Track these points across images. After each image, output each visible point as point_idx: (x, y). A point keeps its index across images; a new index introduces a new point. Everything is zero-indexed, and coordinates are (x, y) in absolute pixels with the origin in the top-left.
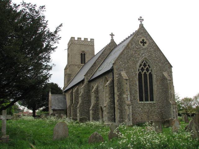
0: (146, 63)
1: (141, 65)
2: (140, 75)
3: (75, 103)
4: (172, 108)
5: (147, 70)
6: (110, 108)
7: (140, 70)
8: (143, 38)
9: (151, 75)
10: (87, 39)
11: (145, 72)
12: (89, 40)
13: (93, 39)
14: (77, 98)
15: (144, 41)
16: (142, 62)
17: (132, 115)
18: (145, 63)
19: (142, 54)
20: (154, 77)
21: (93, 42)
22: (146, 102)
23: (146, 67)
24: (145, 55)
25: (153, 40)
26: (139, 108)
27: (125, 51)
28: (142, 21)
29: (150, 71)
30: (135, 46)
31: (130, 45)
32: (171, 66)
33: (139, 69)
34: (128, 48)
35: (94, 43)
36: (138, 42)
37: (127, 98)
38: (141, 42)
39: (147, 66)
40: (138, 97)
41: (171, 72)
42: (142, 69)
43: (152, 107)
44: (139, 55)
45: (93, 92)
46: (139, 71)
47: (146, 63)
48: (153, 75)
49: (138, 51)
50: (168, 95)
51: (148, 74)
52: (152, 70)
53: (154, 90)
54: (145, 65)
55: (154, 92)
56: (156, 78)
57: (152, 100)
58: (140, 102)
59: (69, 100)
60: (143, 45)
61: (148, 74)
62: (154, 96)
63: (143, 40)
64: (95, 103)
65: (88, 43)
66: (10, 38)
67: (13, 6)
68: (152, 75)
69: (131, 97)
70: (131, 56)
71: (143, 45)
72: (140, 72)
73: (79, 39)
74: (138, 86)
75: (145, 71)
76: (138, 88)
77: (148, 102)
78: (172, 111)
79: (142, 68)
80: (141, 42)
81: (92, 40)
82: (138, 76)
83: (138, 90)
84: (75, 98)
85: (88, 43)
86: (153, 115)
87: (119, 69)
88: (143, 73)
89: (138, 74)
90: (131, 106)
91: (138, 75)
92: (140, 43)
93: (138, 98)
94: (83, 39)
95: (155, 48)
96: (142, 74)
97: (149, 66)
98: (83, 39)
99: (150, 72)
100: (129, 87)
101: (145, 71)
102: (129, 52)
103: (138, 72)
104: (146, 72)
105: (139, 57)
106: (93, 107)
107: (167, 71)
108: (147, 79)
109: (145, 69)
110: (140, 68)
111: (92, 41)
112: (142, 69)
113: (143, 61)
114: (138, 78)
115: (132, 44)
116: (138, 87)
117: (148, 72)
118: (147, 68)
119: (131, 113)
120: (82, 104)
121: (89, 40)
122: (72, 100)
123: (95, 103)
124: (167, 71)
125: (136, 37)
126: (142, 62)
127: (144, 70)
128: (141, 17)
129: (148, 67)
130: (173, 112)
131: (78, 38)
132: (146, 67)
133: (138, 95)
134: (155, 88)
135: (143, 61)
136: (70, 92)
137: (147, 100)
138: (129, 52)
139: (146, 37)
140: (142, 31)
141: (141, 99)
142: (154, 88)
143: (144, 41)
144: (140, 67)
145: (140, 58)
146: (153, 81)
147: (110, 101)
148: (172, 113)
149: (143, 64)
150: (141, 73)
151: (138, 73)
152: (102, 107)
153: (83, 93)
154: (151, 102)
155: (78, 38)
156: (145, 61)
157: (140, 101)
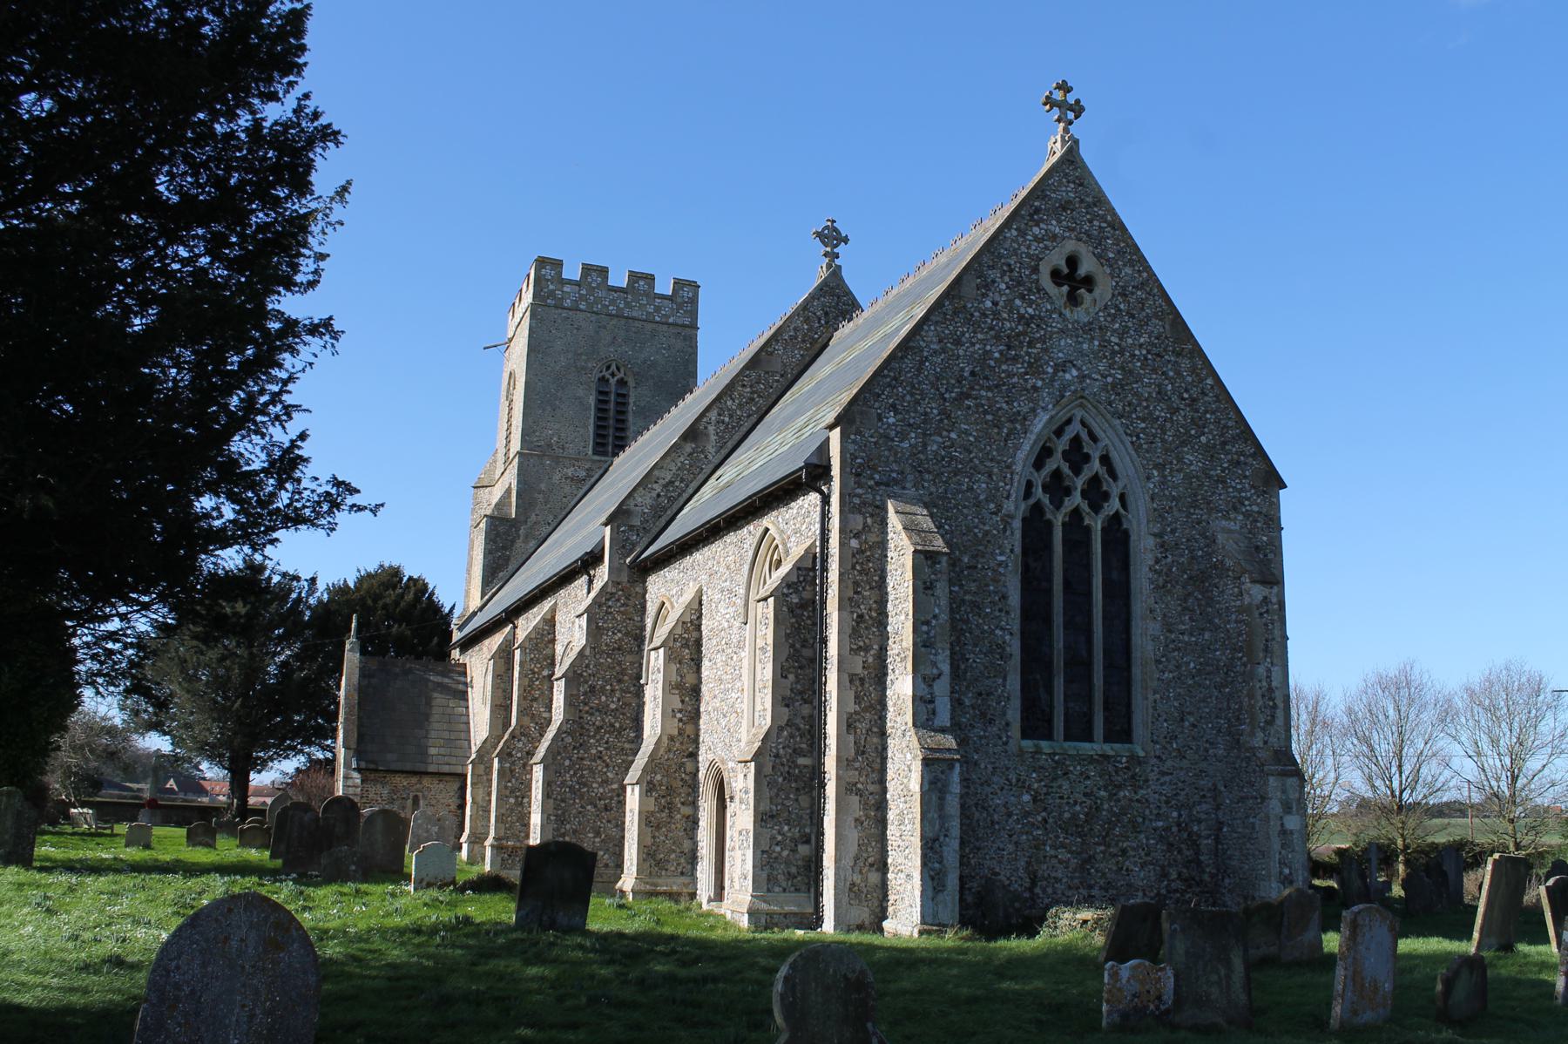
0: (1084, 436)
1: (1045, 453)
2: (1035, 525)
3: (521, 733)
4: (1275, 806)
5: (1095, 493)
6: (788, 777)
7: (1039, 492)
8: (1070, 246)
9: (1117, 535)
10: (650, 278)
11: (1076, 513)
12: (664, 287)
13: (695, 286)
14: (537, 696)
15: (1065, 289)
16: (1059, 432)
17: (962, 843)
18: (1076, 440)
19: (1061, 367)
20: (1144, 546)
21: (694, 301)
22: (1072, 747)
23: (1087, 474)
24: (1082, 377)
25: (1148, 268)
26: (1022, 785)
27: (930, 332)
28: (1071, 115)
29: (1115, 504)
30: (1010, 302)
31: (969, 289)
32: (1272, 481)
33: (1029, 485)
34: (955, 313)
35: (694, 314)
36: (1035, 270)
37: (932, 702)
38: (1056, 275)
39: (1096, 465)
40: (1016, 703)
41: (1272, 523)
42: (1058, 490)
43: (1120, 787)
44: (1035, 368)
45: (656, 649)
46: (1028, 493)
47: (1084, 436)
48: (1133, 537)
49: (1031, 344)
50: (1251, 696)
51: (1096, 524)
52: (1130, 499)
53: (1136, 654)
54: (1076, 455)
55: (1136, 672)
56: (1157, 561)
57: (1120, 731)
58: (1028, 744)
59: (484, 703)
60: (1073, 300)
61: (1096, 524)
62: (919, 909)
63: (1072, 261)
64: (671, 738)
65: (658, 309)
66: (121, 288)
67: (298, 347)
68: (1126, 534)
69: (957, 703)
70: (973, 373)
71: (1073, 300)
72: (1037, 508)
73: (595, 279)
74: (1016, 614)
75: (1076, 499)
76: (1016, 626)
77: (1086, 747)
78: (1274, 826)
79: (1057, 474)
80: (1056, 275)
81: (686, 293)
82: (1018, 535)
83: (1014, 647)
84: (526, 692)
85: (658, 309)
86: (1124, 852)
87: (874, 469)
88: (1059, 520)
89: (1024, 520)
90: (956, 776)
91: (1017, 524)
92: (1046, 281)
93: (1014, 714)
94: (618, 279)
95: (1156, 326)
96: (1049, 525)
97: (1106, 460)
98: (618, 279)
99: (1117, 516)
100: (944, 617)
101: (1076, 499)
102: (958, 343)
103: (1023, 506)
104: (1085, 507)
105: (1035, 388)
106: (653, 764)
107: (1247, 515)
108: (1088, 567)
109: (1080, 483)
110: (1039, 479)
111: (686, 293)
112: (1058, 490)
113: (1069, 421)
114: (1018, 550)
115: (987, 286)
116: (1014, 621)
117: (1096, 508)
118: (1095, 480)
119: (955, 831)
120: (569, 740)
121: (664, 287)
122: (500, 708)
123: (671, 738)
124: (1247, 515)
125: (1022, 233)
126: (1059, 432)
127: (1068, 492)
128: (1064, 87)
129: (1102, 471)
130: (1284, 832)
131: (587, 269)
132: (1087, 474)
133: (1014, 683)
134: (1146, 635)
135: (1069, 421)
136: (496, 640)
137: (1080, 730)
138: (958, 343)
139: (1097, 241)
140: (1068, 192)
141: (1036, 723)
142: (1137, 640)
143: (1065, 289)
144: (1038, 464)
145: (1046, 397)
146: (1134, 585)
147: (789, 724)
148: (1276, 844)
149: (1062, 445)
150: (1049, 516)
151: (1016, 507)
152: (719, 774)
153: (581, 653)
154: (1108, 749)
155: (587, 269)
156: (1083, 423)
157: (1025, 734)
